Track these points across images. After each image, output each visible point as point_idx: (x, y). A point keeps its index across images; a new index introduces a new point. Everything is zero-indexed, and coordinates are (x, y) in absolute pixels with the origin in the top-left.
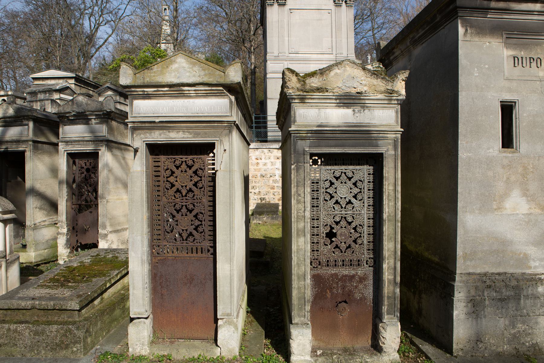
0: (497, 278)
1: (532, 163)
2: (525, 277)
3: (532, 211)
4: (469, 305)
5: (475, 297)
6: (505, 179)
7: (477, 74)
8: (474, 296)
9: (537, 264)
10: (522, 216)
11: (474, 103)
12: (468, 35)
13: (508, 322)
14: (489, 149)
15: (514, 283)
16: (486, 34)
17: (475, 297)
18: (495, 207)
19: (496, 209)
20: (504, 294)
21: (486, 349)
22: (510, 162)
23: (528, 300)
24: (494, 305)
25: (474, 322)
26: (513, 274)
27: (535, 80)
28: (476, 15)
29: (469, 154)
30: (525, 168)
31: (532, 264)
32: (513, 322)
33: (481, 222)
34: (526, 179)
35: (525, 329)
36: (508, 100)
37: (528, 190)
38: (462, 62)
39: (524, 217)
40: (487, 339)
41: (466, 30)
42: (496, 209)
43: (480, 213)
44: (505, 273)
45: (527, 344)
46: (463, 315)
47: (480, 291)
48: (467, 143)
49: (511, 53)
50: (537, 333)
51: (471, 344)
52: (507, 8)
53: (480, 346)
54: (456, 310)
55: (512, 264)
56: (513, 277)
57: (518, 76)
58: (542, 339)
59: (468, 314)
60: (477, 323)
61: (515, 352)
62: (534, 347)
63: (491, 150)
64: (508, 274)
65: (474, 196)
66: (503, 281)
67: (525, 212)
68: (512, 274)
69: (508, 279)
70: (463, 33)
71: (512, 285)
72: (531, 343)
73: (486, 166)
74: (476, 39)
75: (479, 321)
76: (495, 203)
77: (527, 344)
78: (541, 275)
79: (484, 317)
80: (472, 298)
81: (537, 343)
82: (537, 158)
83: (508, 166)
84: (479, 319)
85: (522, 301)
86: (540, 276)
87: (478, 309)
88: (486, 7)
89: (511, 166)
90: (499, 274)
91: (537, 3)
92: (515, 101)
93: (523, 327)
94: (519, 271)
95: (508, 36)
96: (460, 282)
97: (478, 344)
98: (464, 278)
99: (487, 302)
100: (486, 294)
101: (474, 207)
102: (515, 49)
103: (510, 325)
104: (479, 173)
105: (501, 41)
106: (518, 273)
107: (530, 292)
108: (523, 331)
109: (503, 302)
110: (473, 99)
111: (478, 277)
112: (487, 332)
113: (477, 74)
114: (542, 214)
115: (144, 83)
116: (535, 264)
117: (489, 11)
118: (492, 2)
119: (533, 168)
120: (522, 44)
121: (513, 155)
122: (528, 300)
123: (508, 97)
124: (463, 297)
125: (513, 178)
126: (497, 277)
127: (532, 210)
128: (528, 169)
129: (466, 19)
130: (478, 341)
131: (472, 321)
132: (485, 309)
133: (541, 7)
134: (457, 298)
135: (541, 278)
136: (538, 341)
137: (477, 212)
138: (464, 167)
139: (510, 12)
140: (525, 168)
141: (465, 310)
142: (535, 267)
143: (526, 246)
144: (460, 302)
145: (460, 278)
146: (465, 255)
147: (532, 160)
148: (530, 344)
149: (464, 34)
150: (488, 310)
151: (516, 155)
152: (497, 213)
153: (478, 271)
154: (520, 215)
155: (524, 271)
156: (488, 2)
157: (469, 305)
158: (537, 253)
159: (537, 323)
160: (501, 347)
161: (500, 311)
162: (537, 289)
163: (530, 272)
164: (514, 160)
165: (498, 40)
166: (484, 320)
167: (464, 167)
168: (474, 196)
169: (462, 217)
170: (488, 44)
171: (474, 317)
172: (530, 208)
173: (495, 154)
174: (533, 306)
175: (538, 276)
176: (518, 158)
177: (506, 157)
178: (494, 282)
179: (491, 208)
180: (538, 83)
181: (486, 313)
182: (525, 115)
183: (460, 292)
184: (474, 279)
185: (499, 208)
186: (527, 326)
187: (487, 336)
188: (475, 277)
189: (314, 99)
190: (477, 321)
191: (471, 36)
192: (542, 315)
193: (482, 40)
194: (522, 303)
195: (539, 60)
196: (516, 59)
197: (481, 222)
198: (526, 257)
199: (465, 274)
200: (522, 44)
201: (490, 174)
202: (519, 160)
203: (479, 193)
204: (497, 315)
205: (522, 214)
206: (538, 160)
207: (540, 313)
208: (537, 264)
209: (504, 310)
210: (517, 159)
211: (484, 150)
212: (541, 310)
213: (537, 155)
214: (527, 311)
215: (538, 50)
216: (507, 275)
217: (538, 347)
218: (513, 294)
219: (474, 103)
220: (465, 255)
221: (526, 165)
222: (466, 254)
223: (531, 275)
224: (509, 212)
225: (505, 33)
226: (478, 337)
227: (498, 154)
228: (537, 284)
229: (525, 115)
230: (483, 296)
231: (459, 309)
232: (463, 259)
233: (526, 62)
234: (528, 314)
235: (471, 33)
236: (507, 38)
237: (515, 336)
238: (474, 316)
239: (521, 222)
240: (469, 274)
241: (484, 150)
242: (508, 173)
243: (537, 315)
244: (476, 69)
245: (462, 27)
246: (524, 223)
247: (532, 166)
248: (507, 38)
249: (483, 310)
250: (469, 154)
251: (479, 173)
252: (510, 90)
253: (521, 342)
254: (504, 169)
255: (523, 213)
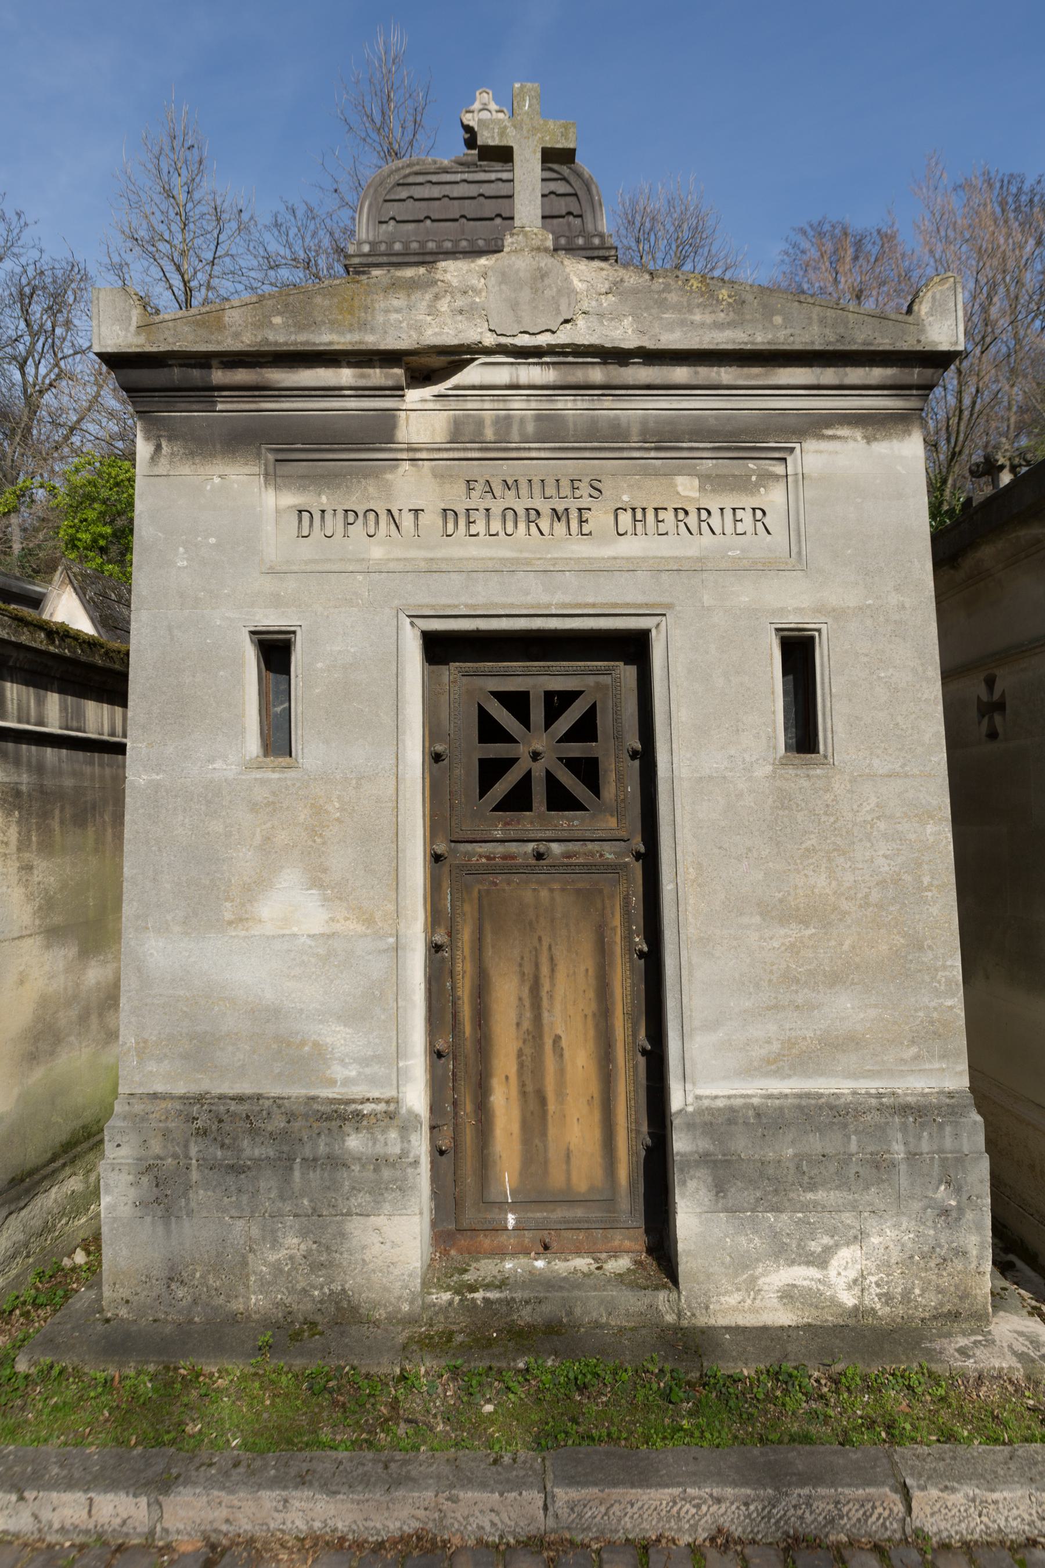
0: (232, 1108)
1: (339, 797)
2: (316, 1107)
3: (337, 927)
4: (145, 1179)
5: (161, 1159)
6: (258, 840)
7: (185, 563)
8: (159, 1157)
9: (354, 1073)
10: (309, 942)
11: (172, 639)
12: (163, 461)
13: (257, 1231)
14: (211, 760)
15: (278, 1123)
16: (213, 455)
17: (161, 1159)
18: (228, 916)
19: (230, 923)
20: (248, 1152)
21: (195, 1302)
22: (274, 793)
23: (314, 1171)
24: (214, 1183)
25: (160, 1229)
26: (283, 1098)
27: (351, 569)
28: (183, 406)
29: (155, 777)
30: (318, 810)
31: (338, 1072)
32: (274, 1232)
33: (189, 956)
34: (319, 840)
35: (310, 1251)
36: (271, 629)
37: (325, 871)
38: (144, 533)
39: (313, 944)
40: (198, 1275)
41: (158, 448)
42: (230, 923)
43: (186, 933)
44: (259, 1097)
45: (316, 1293)
46: (126, 1207)
47: (178, 1144)
48: (150, 745)
49: (291, 499)
50: (345, 1264)
51: (151, 1287)
52: (261, 384)
53: (180, 1294)
54: (107, 1192)
55: (277, 1071)
56: (279, 1107)
57: (307, 562)
58: (358, 1279)
59: (141, 1204)
60: (168, 1232)
61: (280, 1315)
62: (336, 1303)
63: (218, 764)
64: (268, 1098)
65: (168, 886)
66: (248, 1117)
67: (316, 930)
68: (275, 1099)
69: (264, 1112)
70: (148, 456)
71: (270, 1128)
72: (327, 1291)
73: (203, 808)
74: (186, 469)
75: (173, 1225)
76: (228, 904)
77: (316, 1293)
78: (362, 1103)
79: (188, 1215)
80: (151, 1162)
81: (343, 1290)
82: (354, 782)
83: (268, 804)
84: (173, 1219)
85: (297, 1174)
86: (360, 1107)
87: (169, 1192)
88: (200, 384)
89: (278, 805)
90: (240, 1099)
91: (340, 367)
92: (292, 629)
93: (303, 1247)
94: (297, 1091)
95: (280, 456)
96: (125, 1118)
97: (173, 1287)
98: (138, 1108)
99: (195, 1175)
100: (193, 1151)
101: (169, 917)
102: (302, 488)
103: (264, 1239)
104: (183, 825)
105: (256, 470)
106: (297, 1098)
107: (322, 1149)
108: (305, 1257)
109: (243, 1176)
110: (170, 628)
111: (178, 1106)
112: (197, 1256)
113: (185, 563)
114: (366, 936)
115: (869, 440)
116: (346, 1073)
117: (216, 394)
118: (214, 371)
119: (342, 809)
120: (322, 476)
121: (282, 776)
122: (314, 1171)
123: (272, 620)
124: (127, 1158)
125: (282, 838)
126: (233, 1107)
127: (339, 925)
128: (327, 812)
129: (157, 418)
130: (171, 1279)
131: (153, 1223)
132: (191, 1194)
133: (354, 376)
134: (109, 1161)
135: (361, 1111)
136: (347, 1286)
137: (177, 929)
138: (141, 811)
139: (276, 393)
140: (318, 810)
141: (132, 1193)
142: (347, 1082)
143: (321, 1022)
144: (116, 1172)
145: (127, 1108)
146: (142, 1045)
147: (339, 787)
148: (324, 1294)
149: (152, 458)
150: (200, 1195)
151: (291, 774)
152: (234, 934)
153: (180, 1089)
154: (303, 939)
155: (313, 1092)
156: (205, 371)
157: (145, 1179)
158: (353, 1042)
159: (343, 1235)
160: (241, 1300)
161: (234, 1199)
162: (344, 1141)
163: (331, 1096)
164: (287, 788)
165: (247, 470)
166: (186, 1222)
167: (141, 811)
168: (168, 886)
169: (132, 943)
170: (217, 480)
171: (160, 1214)
172: (332, 919)
173: (230, 775)
174: (329, 1188)
175: (353, 1107)
176: (298, 784)
177: (263, 782)
178: (221, 1121)
179: (218, 920)
180: (360, 577)
181: (193, 1204)
182: (319, 665)
183: (119, 1145)
184: (168, 1112)
185: (241, 920)
186: (315, 1242)
187: (197, 1267)
188: (169, 1105)
189: (799, 542)
190: (167, 1224)
191: (171, 462)
192: (357, 1214)
193: (201, 470)
194: (298, 1180)
195: (372, 515)
196: (305, 515)
197: (189, 956)
198: (320, 1053)
199: (141, 1097)
200: (322, 476)
201: (216, 826)
202: (300, 788)
203: (184, 878)
204: (225, 1211)
205: (309, 936)
206: (358, 787)
207: (349, 1209)
208: (352, 1072)
209: (245, 1198)
210: (294, 785)
211: (199, 764)
212: (353, 1200)
213: (354, 775)
214: (311, 1201)
215: (371, 489)
216: (261, 1102)
217: (349, 1301)
218: (271, 1153)
219: (172, 639)
220: (142, 1045)
221: (321, 802)
222: (145, 1042)
223: (331, 1103)
224: (269, 929)
225: (268, 449)
226: (172, 1269)
227: (240, 774)
228: (345, 1128)
229: (319, 665)
230: (188, 1157)
231: (116, 1190)
232: (138, 1056)
233: (334, 524)
234: (314, 1210)
235: (172, 454)
236: (277, 461)
237: (281, 1271)
238: (159, 1211)
239: (305, 958)
240: (155, 1096)
241: (199, 764)
242: (269, 825)
243: (342, 1215)
244: (181, 550)
245: (147, 439)
246: (313, 960)
247: (337, 805)
248: (277, 461)
249: (185, 1194)
250: (155, 777)
251: (183, 825)
252: (277, 601)
253: (299, 1287)
254: (257, 812)
255: (312, 932)
